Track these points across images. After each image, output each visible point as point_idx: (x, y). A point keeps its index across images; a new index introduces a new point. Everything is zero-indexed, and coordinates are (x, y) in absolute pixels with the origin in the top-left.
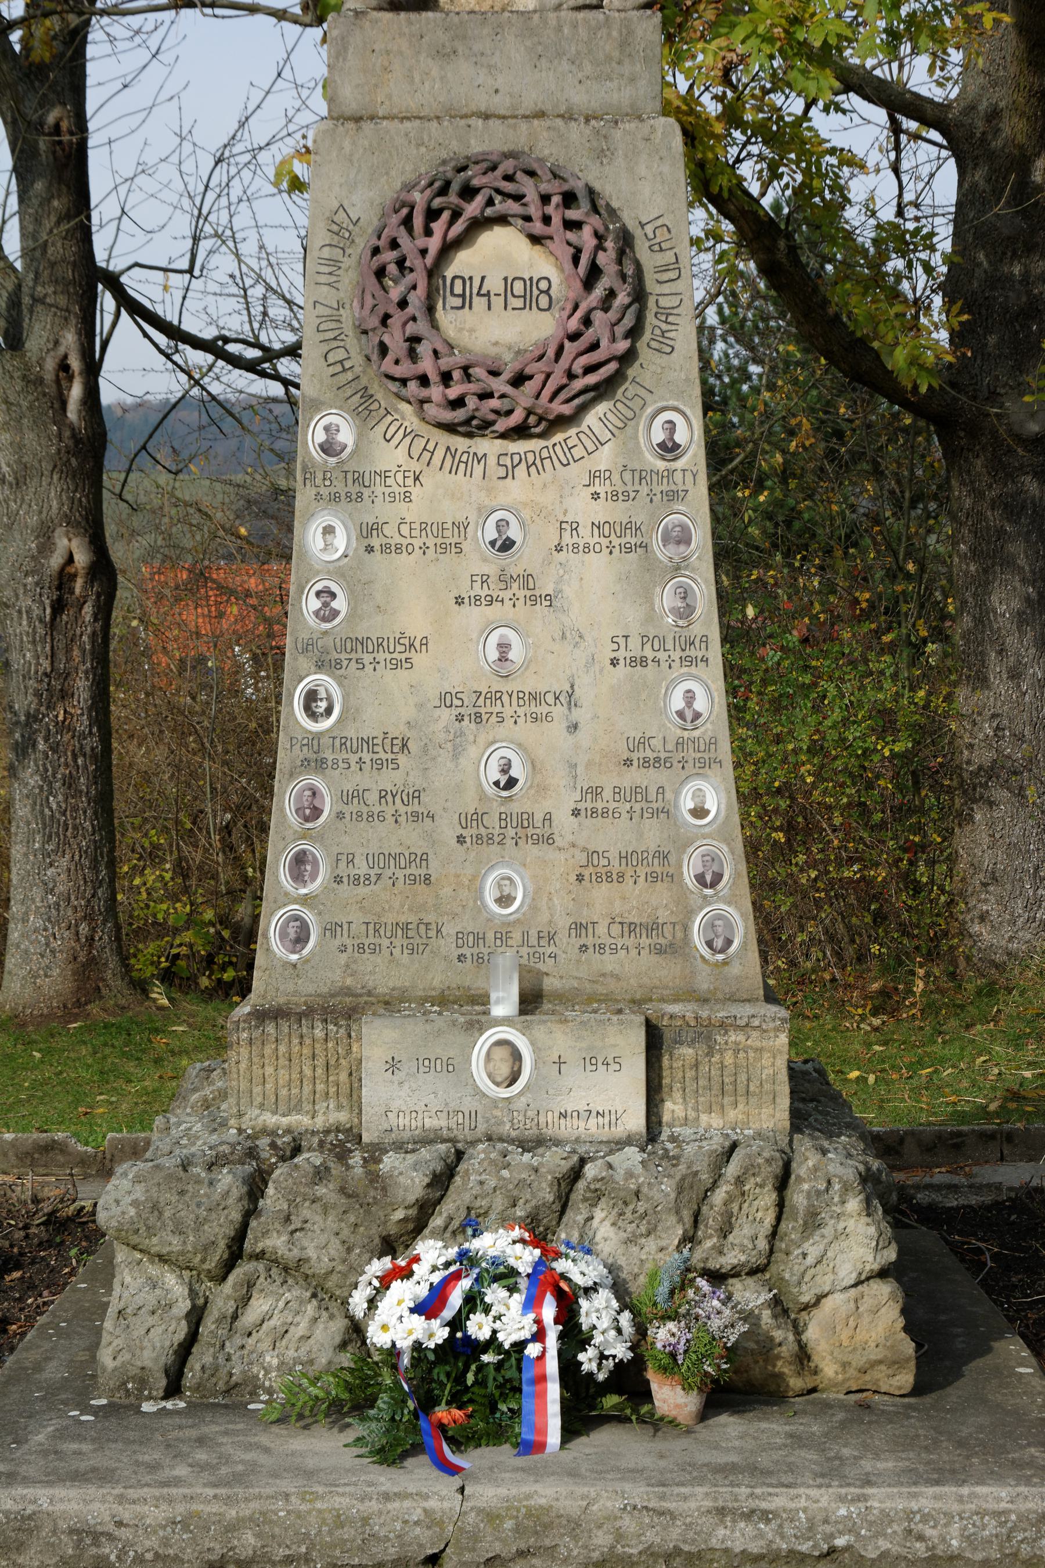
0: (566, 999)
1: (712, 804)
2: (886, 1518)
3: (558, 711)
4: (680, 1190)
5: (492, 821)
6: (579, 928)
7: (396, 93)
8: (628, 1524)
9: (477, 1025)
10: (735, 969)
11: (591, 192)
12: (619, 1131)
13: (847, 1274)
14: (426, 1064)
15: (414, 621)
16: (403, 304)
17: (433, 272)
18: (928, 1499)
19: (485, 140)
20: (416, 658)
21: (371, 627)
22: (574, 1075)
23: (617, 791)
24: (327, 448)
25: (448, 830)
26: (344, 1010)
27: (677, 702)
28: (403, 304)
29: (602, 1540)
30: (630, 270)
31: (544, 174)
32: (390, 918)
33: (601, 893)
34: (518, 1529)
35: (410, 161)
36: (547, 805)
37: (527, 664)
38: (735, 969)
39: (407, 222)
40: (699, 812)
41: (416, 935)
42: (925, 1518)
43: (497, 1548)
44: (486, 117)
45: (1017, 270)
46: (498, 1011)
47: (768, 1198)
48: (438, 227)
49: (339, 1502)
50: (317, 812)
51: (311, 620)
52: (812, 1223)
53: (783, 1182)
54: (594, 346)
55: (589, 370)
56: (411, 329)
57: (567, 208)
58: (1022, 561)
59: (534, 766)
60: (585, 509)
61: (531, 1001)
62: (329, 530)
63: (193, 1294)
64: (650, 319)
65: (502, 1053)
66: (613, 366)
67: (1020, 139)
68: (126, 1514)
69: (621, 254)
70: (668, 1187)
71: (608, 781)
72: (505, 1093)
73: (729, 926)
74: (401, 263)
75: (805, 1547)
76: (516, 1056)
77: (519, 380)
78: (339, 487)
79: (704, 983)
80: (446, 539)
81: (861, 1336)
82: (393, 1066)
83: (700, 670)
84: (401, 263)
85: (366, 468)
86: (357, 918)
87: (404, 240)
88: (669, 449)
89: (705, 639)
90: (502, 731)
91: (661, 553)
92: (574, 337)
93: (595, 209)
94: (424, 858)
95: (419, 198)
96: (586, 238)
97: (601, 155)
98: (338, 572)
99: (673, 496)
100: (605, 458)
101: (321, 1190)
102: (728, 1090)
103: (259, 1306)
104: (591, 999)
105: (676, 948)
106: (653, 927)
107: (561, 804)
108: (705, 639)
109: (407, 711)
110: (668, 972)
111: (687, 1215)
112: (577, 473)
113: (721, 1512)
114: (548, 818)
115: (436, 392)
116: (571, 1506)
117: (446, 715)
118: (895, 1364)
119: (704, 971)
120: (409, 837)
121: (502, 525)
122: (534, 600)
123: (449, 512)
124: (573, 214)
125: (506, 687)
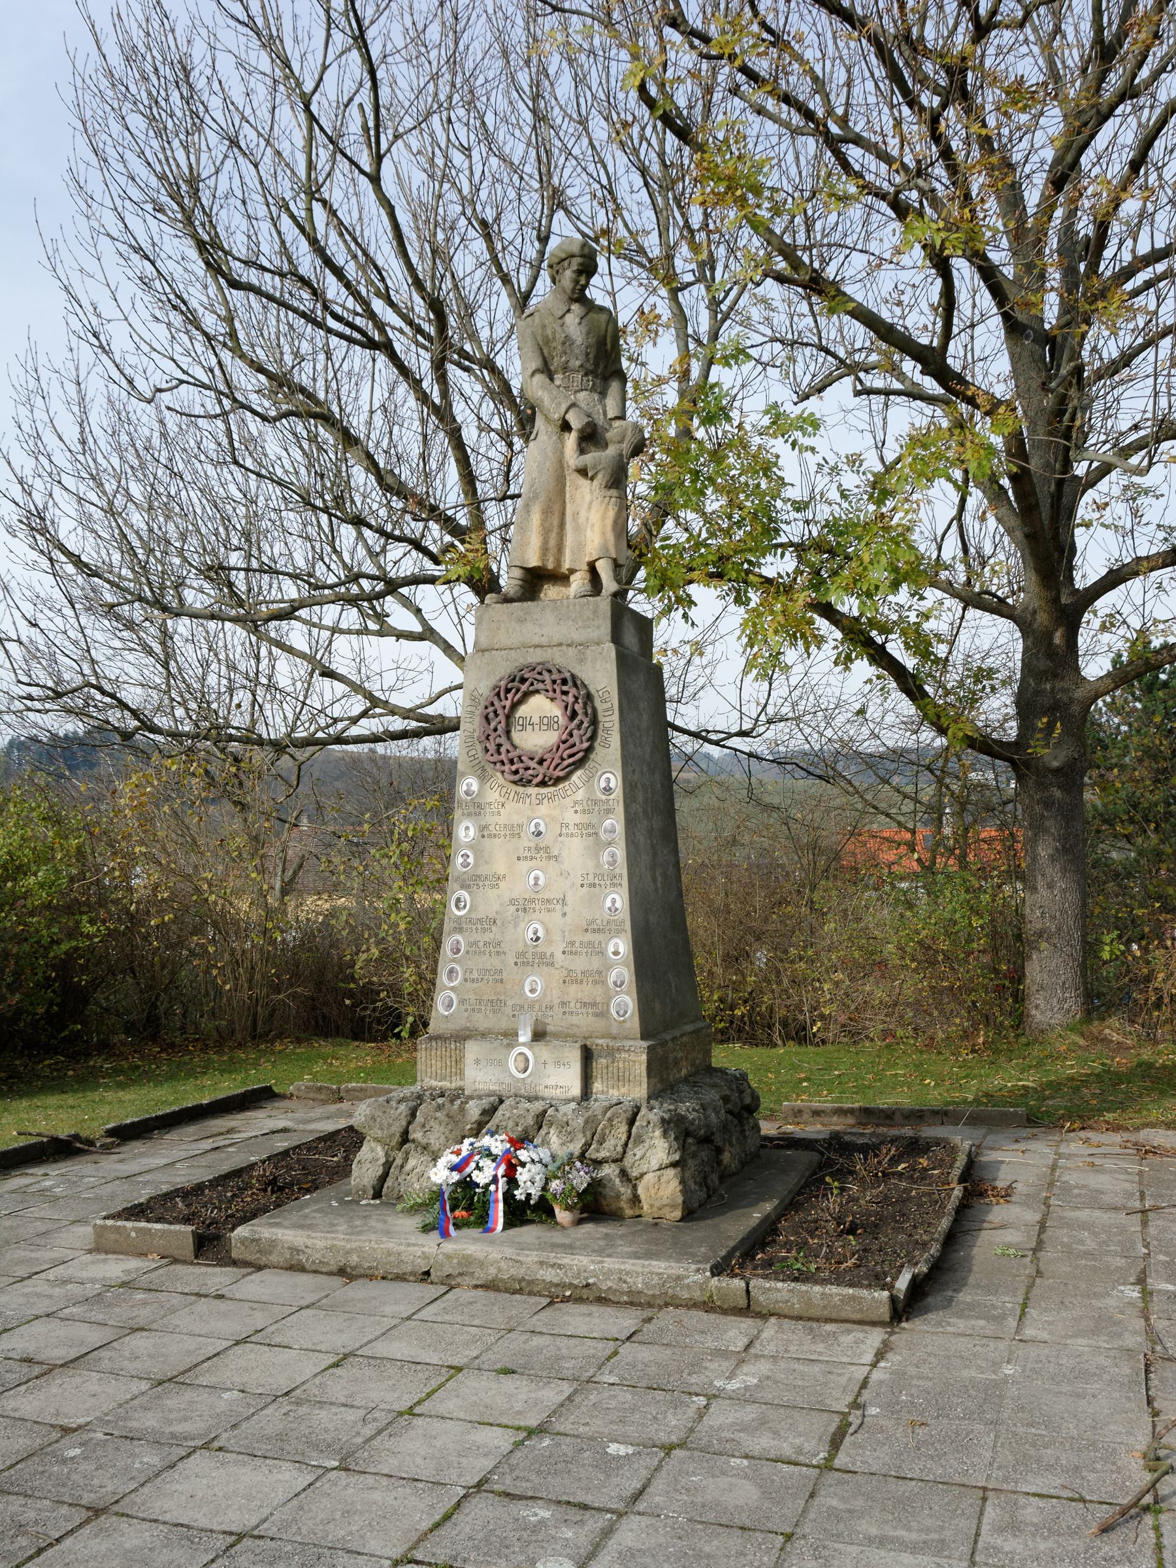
0: (556, 1036)
1: (621, 950)
2: (610, 1272)
3: (559, 907)
4: (586, 1122)
5: (529, 956)
6: (563, 1004)
7: (503, 639)
8: (503, 1265)
9: (511, 1046)
10: (628, 1025)
11: (573, 677)
12: (569, 1095)
13: (655, 1164)
14: (491, 1062)
15: (500, 867)
16: (495, 730)
17: (508, 717)
18: (629, 1265)
19: (535, 657)
20: (501, 884)
21: (483, 870)
22: (551, 1069)
23: (581, 943)
24: (467, 793)
25: (511, 959)
26: (462, 1037)
27: (608, 904)
28: (495, 730)
29: (493, 1271)
30: (589, 711)
31: (554, 671)
32: (485, 998)
33: (573, 988)
34: (459, 1263)
35: (503, 667)
36: (552, 949)
37: (545, 887)
38: (628, 1025)
39: (498, 694)
40: (616, 953)
41: (496, 1005)
42: (627, 1273)
43: (451, 1271)
44: (536, 646)
45: (1048, 686)
46: (522, 1039)
47: (624, 1128)
48: (510, 696)
49: (390, 1245)
50: (458, 950)
51: (459, 867)
52: (640, 1140)
53: (631, 1122)
54: (574, 745)
55: (570, 756)
56: (498, 740)
57: (568, 686)
58: (1053, 830)
59: (547, 930)
60: (572, 818)
61: (539, 1035)
62: (467, 828)
63: (387, 1154)
64: (600, 732)
65: (521, 1058)
66: (581, 755)
67: (1046, 623)
68: (309, 1242)
69: (585, 704)
70: (581, 1121)
71: (578, 939)
72: (522, 1076)
73: (626, 1005)
74: (495, 712)
75: (576, 1282)
76: (527, 1060)
77: (541, 762)
78: (472, 809)
79: (614, 1031)
80: (514, 832)
81: (661, 1193)
82: (477, 1062)
83: (618, 889)
84: (495, 712)
85: (482, 801)
86: (472, 997)
87: (496, 703)
88: (608, 790)
89: (621, 875)
90: (534, 916)
91: (603, 837)
92: (564, 742)
93: (575, 685)
94: (501, 971)
95: (503, 683)
96: (570, 699)
97: (581, 661)
98: (470, 846)
99: (609, 811)
100: (580, 795)
101: (438, 1114)
102: (621, 1079)
103: (412, 1162)
104: (567, 1036)
105: (603, 1014)
106: (594, 1004)
107: (557, 948)
108: (621, 875)
109: (496, 907)
110: (599, 1025)
111: (589, 1134)
112: (568, 802)
113: (542, 1263)
114: (552, 955)
115: (507, 768)
116: (480, 1255)
117: (512, 909)
118: (673, 1206)
119: (615, 1025)
120: (496, 962)
121: (537, 825)
122: (549, 858)
123: (516, 819)
124: (565, 688)
125: (540, 896)
